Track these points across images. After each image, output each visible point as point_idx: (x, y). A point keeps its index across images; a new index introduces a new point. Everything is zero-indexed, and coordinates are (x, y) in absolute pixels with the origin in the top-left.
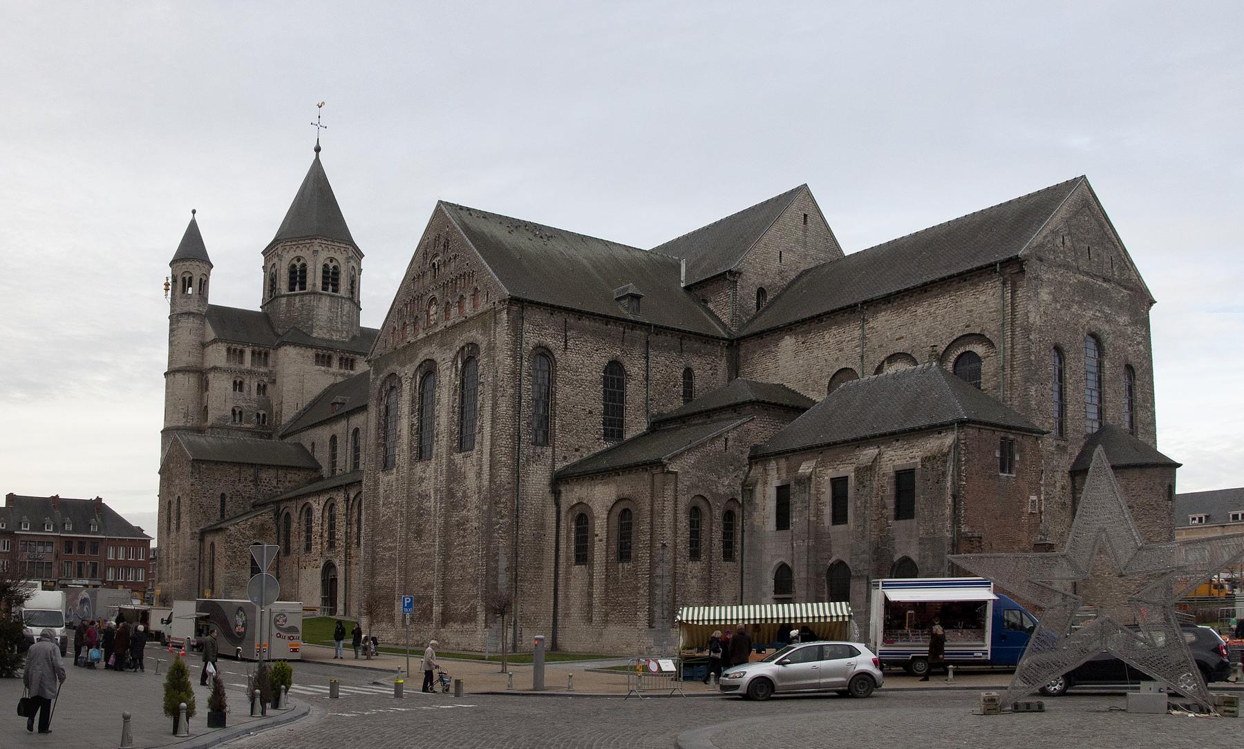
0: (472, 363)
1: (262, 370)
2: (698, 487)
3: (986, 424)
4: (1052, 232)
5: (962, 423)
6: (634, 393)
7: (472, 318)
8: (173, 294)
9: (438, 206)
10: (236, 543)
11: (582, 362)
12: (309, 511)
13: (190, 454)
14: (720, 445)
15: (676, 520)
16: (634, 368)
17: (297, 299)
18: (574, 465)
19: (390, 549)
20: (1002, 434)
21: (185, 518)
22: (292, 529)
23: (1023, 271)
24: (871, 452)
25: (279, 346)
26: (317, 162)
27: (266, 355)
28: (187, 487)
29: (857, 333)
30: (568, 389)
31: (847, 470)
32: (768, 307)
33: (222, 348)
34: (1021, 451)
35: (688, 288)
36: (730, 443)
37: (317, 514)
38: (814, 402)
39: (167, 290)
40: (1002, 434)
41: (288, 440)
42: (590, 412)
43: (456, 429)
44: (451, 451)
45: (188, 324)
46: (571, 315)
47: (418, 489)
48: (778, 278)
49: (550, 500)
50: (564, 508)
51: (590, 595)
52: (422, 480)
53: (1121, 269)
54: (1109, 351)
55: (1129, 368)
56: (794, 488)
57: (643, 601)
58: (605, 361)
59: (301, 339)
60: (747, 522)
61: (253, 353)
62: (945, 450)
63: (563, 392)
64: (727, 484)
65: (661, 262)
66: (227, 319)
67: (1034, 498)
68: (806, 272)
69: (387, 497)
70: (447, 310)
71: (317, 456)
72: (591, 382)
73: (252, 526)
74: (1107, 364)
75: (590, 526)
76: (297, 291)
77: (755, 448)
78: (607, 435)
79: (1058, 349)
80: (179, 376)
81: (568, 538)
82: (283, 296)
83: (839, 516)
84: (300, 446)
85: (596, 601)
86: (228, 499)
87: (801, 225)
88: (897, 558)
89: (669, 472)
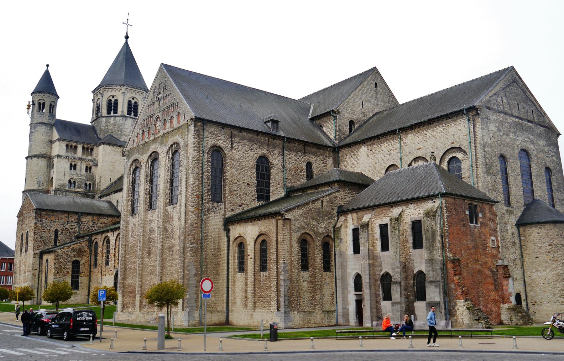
0: (177, 154)
1: (89, 158)
2: (304, 228)
3: (458, 195)
6: (276, 175)
7: (176, 129)
8: (32, 112)
10: (62, 260)
14: (318, 204)
15: (291, 247)
16: (275, 160)
17: (112, 119)
18: (236, 215)
19: (135, 263)
20: (470, 202)
21: (31, 245)
22: (99, 252)
23: (478, 114)
24: (396, 211)
25: (100, 145)
26: (126, 44)
28: (33, 225)
32: (355, 131)
33: (64, 144)
34: (482, 212)
36: (325, 204)
39: (28, 109)
40: (470, 202)
41: (104, 199)
42: (248, 184)
44: (166, 204)
45: (41, 129)
47: (148, 227)
49: (224, 234)
50: (232, 239)
51: (246, 291)
53: (539, 116)
57: (274, 295)
59: (113, 142)
60: (337, 249)
61: (83, 148)
63: (230, 173)
64: (322, 227)
65: (301, 105)
66: (69, 129)
67: (494, 238)
68: (377, 113)
69: (133, 232)
70: (164, 124)
71: (120, 209)
72: (248, 167)
73: (73, 250)
74: (533, 166)
75: (245, 249)
77: (340, 207)
78: (259, 198)
80: (35, 159)
82: (104, 117)
83: (385, 247)
84: (110, 202)
85: (249, 295)
86: (59, 233)
87: (374, 89)
88: (416, 271)
89: (285, 219)
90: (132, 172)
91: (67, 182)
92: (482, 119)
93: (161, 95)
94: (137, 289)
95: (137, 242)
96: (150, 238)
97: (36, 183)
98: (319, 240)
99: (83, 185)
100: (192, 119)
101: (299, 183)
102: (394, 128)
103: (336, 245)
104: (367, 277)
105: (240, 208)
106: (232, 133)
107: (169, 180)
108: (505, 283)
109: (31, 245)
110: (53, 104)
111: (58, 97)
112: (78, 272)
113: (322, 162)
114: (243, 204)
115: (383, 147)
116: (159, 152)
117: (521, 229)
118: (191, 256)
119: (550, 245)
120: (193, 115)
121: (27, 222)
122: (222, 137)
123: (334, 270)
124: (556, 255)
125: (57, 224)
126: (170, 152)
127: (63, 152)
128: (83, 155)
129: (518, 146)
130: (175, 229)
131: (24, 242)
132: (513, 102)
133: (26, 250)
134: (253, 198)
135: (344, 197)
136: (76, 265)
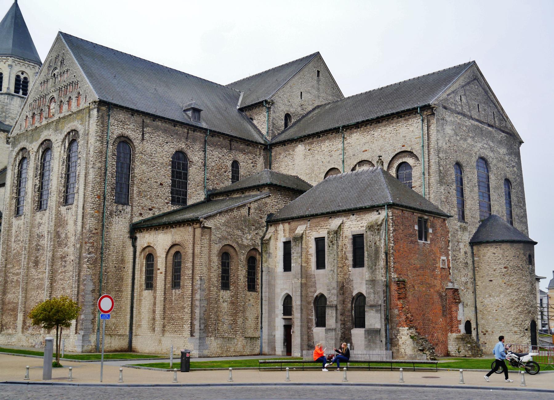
0: (75, 144)
2: (227, 239)
3: (406, 207)
6: (195, 174)
7: (74, 113)
9: (58, 35)
14: (244, 211)
15: (210, 261)
16: (195, 156)
18: (145, 221)
19: (18, 274)
20: (419, 215)
23: (433, 114)
24: (335, 223)
30: (144, 167)
31: (323, 233)
32: (292, 126)
36: (252, 211)
38: (311, 186)
40: (419, 215)
42: (161, 184)
44: (59, 204)
47: (36, 231)
48: (299, 109)
49: (129, 242)
50: (139, 249)
51: (154, 312)
52: (40, 224)
53: (500, 120)
57: (187, 317)
58: (173, 151)
60: (265, 265)
62: (379, 223)
64: (248, 239)
68: (318, 107)
69: (17, 236)
70: (60, 107)
72: (162, 163)
74: (492, 177)
75: (155, 262)
77: (270, 215)
78: (174, 201)
79: (458, 165)
81: (141, 270)
83: (321, 264)
85: (158, 316)
87: (316, 78)
88: (354, 294)
89: (205, 227)
90: (17, 163)
92: (438, 120)
93: (57, 71)
94: (20, 306)
95: (21, 249)
96: (38, 245)
98: (244, 254)
100: (95, 102)
101: (222, 185)
102: (337, 126)
105: (150, 212)
106: (143, 121)
107: (64, 175)
108: (454, 309)
113: (251, 161)
114: (153, 207)
115: (323, 146)
116: (53, 140)
119: (505, 268)
122: (131, 126)
123: (260, 290)
124: (511, 278)
126: (67, 141)
129: (476, 153)
130: (69, 235)
132: (473, 102)
134: (166, 201)
135: (275, 203)
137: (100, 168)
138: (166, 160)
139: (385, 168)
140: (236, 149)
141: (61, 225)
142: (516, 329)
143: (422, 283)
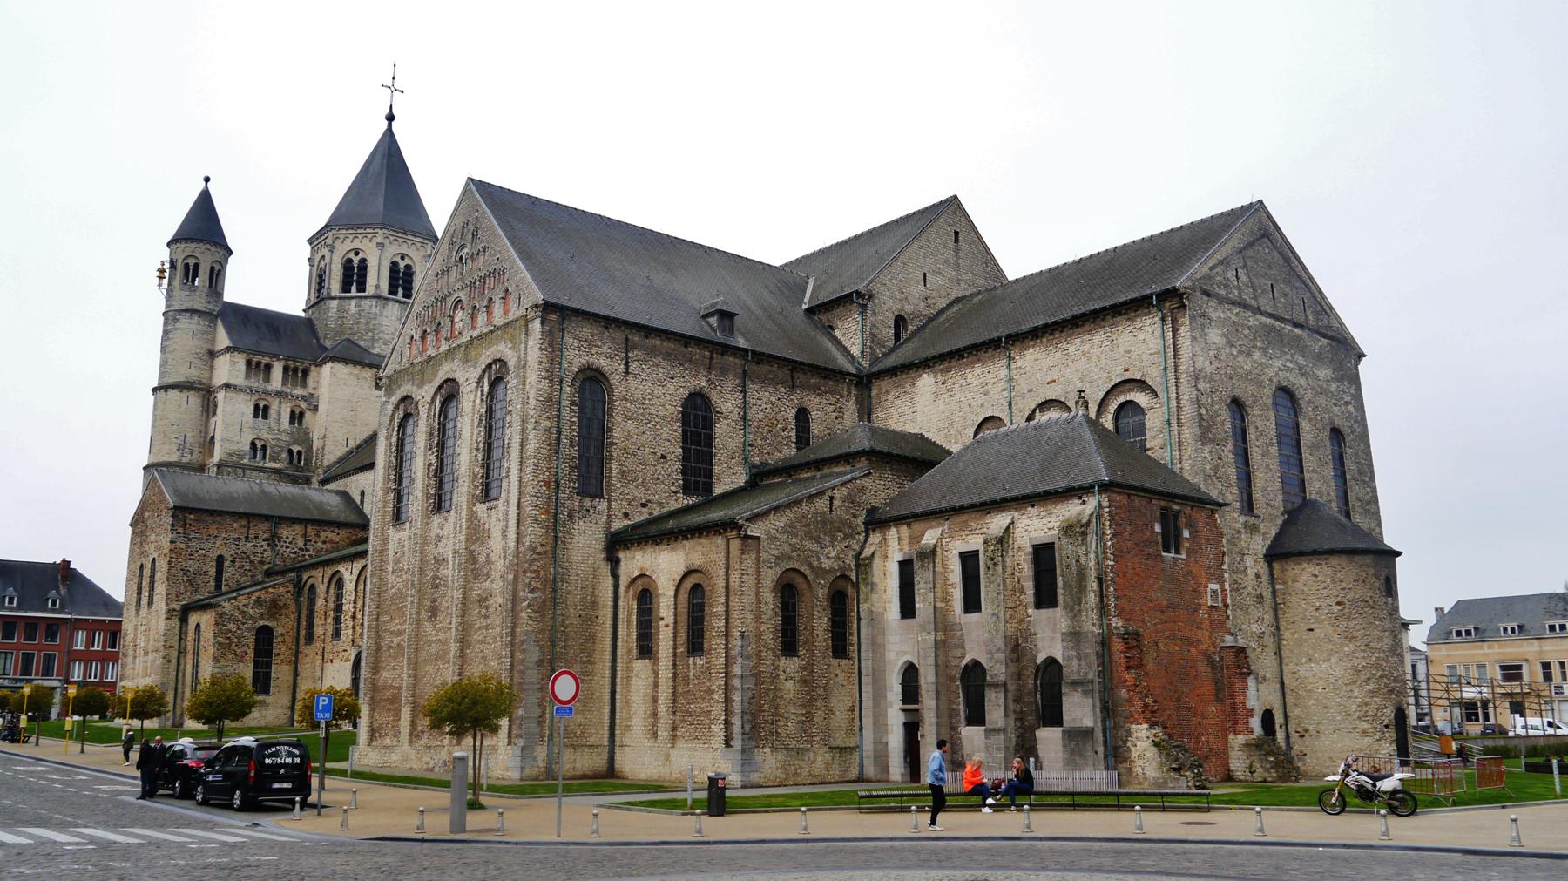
0: (501, 386)
1: (299, 391)
3: (1136, 489)
4: (1221, 262)
5: (1105, 487)
6: (726, 436)
7: (499, 328)
10: (231, 626)
11: (649, 398)
12: (340, 584)
13: (181, 505)
14: (822, 504)
15: (759, 601)
16: (726, 402)
17: (353, 302)
19: (400, 633)
20: (1163, 503)
21: (161, 589)
24: (997, 523)
25: (324, 362)
26: (389, 133)
27: (306, 372)
28: (166, 545)
29: (1003, 373)
30: (630, 425)
31: (975, 543)
32: (908, 340)
33: (240, 360)
35: (811, 311)
36: (837, 503)
37: (349, 586)
38: (949, 453)
39: (161, 278)
40: (1163, 503)
41: (332, 486)
42: (663, 457)
43: (480, 471)
44: (474, 500)
45: (188, 325)
46: (636, 334)
47: (433, 551)
48: (922, 305)
49: (605, 569)
50: (624, 581)
51: (655, 700)
52: (439, 538)
53: (1316, 313)
54: (1307, 409)
55: (1336, 433)
56: (917, 565)
57: (718, 709)
59: (355, 355)
60: (864, 606)
61: (286, 369)
63: (622, 429)
64: (830, 557)
66: (258, 330)
68: (958, 300)
69: (397, 562)
70: (473, 317)
71: (367, 509)
72: (664, 417)
73: (258, 602)
76: (354, 292)
77: (872, 511)
78: (687, 489)
80: (173, 393)
81: (629, 621)
83: (972, 603)
84: (344, 495)
85: (662, 709)
87: (952, 245)
88: (1040, 659)
91: (247, 448)
92: (1193, 317)
97: (175, 448)
99: (284, 455)
101: (778, 455)
103: (862, 596)
104: (932, 670)
108: (1238, 687)
109: (161, 589)
110: (217, 267)
111: (230, 253)
112: (269, 653)
116: (461, 380)
117: (1276, 565)
118: (530, 618)
119: (1338, 603)
120: (539, 298)
121: (153, 537)
123: (855, 655)
124: (1351, 624)
125: (221, 543)
127: (239, 378)
128: (284, 384)
131: (145, 584)
132: (1262, 281)
133: (150, 603)
136: (264, 637)
137: (548, 430)
138: (671, 410)
139: (1093, 415)
140: (803, 386)
141: (477, 539)
142: (1365, 725)
143: (1172, 637)
